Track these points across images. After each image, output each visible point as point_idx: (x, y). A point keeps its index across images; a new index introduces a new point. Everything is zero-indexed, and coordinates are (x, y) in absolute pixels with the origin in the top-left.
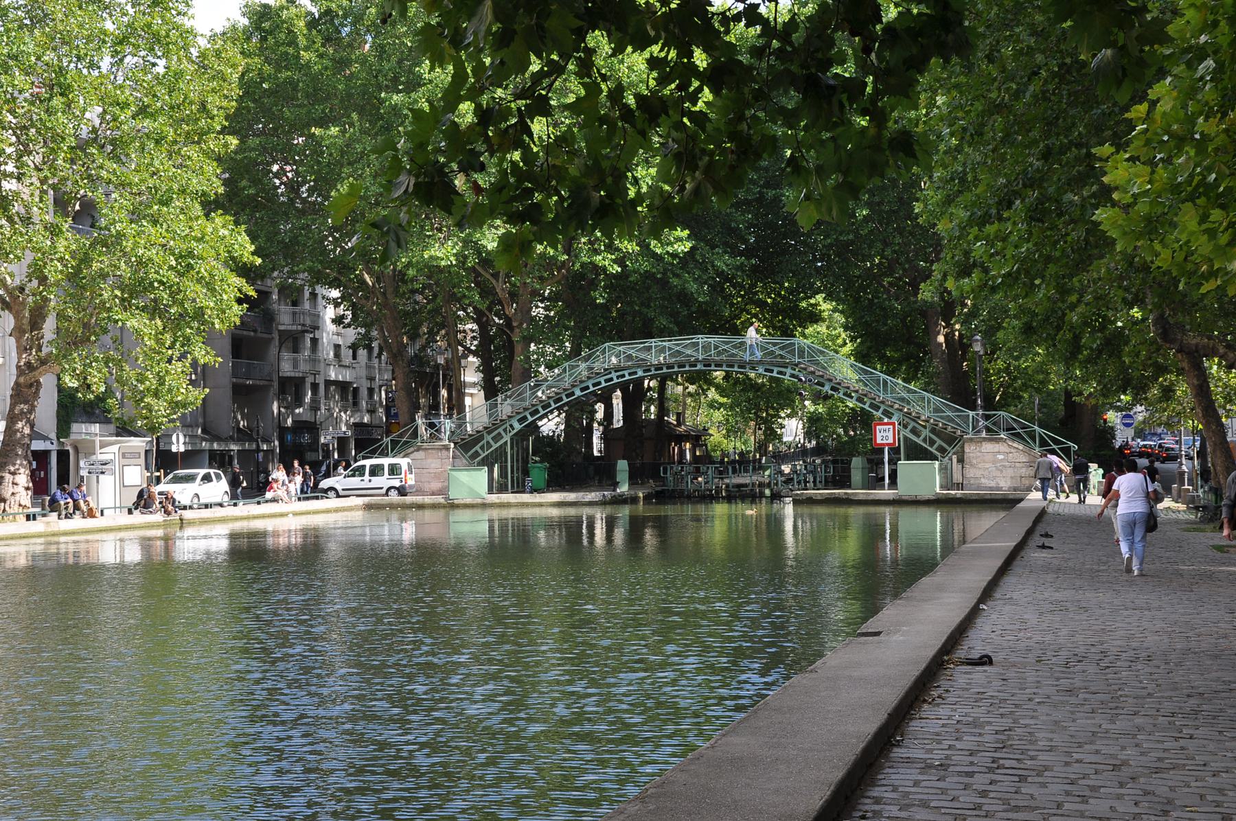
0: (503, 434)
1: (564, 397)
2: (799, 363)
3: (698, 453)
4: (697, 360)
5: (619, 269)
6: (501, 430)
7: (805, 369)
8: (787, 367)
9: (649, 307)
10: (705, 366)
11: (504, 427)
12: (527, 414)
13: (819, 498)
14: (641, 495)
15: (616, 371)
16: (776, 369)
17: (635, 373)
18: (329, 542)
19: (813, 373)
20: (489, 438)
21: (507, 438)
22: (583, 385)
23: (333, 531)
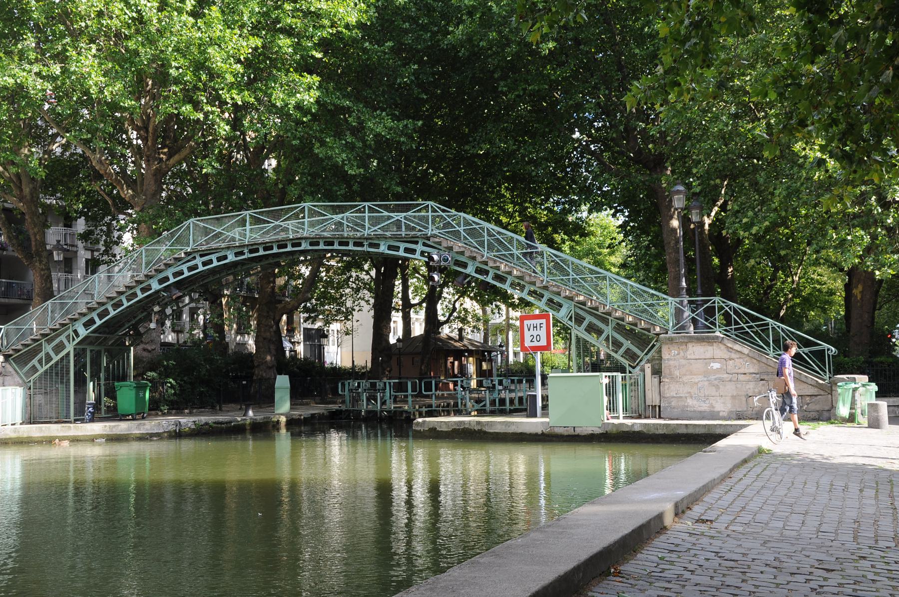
0: (38, 366)
1: (139, 293)
6: (63, 338)
7: (440, 243)
8: (416, 243)
10: (311, 244)
11: (66, 334)
12: (94, 315)
13: (445, 429)
15: (201, 256)
16: (403, 246)
17: (225, 257)
19: (450, 249)
20: (48, 348)
21: (70, 348)
22: (161, 276)
23: (27, 416)
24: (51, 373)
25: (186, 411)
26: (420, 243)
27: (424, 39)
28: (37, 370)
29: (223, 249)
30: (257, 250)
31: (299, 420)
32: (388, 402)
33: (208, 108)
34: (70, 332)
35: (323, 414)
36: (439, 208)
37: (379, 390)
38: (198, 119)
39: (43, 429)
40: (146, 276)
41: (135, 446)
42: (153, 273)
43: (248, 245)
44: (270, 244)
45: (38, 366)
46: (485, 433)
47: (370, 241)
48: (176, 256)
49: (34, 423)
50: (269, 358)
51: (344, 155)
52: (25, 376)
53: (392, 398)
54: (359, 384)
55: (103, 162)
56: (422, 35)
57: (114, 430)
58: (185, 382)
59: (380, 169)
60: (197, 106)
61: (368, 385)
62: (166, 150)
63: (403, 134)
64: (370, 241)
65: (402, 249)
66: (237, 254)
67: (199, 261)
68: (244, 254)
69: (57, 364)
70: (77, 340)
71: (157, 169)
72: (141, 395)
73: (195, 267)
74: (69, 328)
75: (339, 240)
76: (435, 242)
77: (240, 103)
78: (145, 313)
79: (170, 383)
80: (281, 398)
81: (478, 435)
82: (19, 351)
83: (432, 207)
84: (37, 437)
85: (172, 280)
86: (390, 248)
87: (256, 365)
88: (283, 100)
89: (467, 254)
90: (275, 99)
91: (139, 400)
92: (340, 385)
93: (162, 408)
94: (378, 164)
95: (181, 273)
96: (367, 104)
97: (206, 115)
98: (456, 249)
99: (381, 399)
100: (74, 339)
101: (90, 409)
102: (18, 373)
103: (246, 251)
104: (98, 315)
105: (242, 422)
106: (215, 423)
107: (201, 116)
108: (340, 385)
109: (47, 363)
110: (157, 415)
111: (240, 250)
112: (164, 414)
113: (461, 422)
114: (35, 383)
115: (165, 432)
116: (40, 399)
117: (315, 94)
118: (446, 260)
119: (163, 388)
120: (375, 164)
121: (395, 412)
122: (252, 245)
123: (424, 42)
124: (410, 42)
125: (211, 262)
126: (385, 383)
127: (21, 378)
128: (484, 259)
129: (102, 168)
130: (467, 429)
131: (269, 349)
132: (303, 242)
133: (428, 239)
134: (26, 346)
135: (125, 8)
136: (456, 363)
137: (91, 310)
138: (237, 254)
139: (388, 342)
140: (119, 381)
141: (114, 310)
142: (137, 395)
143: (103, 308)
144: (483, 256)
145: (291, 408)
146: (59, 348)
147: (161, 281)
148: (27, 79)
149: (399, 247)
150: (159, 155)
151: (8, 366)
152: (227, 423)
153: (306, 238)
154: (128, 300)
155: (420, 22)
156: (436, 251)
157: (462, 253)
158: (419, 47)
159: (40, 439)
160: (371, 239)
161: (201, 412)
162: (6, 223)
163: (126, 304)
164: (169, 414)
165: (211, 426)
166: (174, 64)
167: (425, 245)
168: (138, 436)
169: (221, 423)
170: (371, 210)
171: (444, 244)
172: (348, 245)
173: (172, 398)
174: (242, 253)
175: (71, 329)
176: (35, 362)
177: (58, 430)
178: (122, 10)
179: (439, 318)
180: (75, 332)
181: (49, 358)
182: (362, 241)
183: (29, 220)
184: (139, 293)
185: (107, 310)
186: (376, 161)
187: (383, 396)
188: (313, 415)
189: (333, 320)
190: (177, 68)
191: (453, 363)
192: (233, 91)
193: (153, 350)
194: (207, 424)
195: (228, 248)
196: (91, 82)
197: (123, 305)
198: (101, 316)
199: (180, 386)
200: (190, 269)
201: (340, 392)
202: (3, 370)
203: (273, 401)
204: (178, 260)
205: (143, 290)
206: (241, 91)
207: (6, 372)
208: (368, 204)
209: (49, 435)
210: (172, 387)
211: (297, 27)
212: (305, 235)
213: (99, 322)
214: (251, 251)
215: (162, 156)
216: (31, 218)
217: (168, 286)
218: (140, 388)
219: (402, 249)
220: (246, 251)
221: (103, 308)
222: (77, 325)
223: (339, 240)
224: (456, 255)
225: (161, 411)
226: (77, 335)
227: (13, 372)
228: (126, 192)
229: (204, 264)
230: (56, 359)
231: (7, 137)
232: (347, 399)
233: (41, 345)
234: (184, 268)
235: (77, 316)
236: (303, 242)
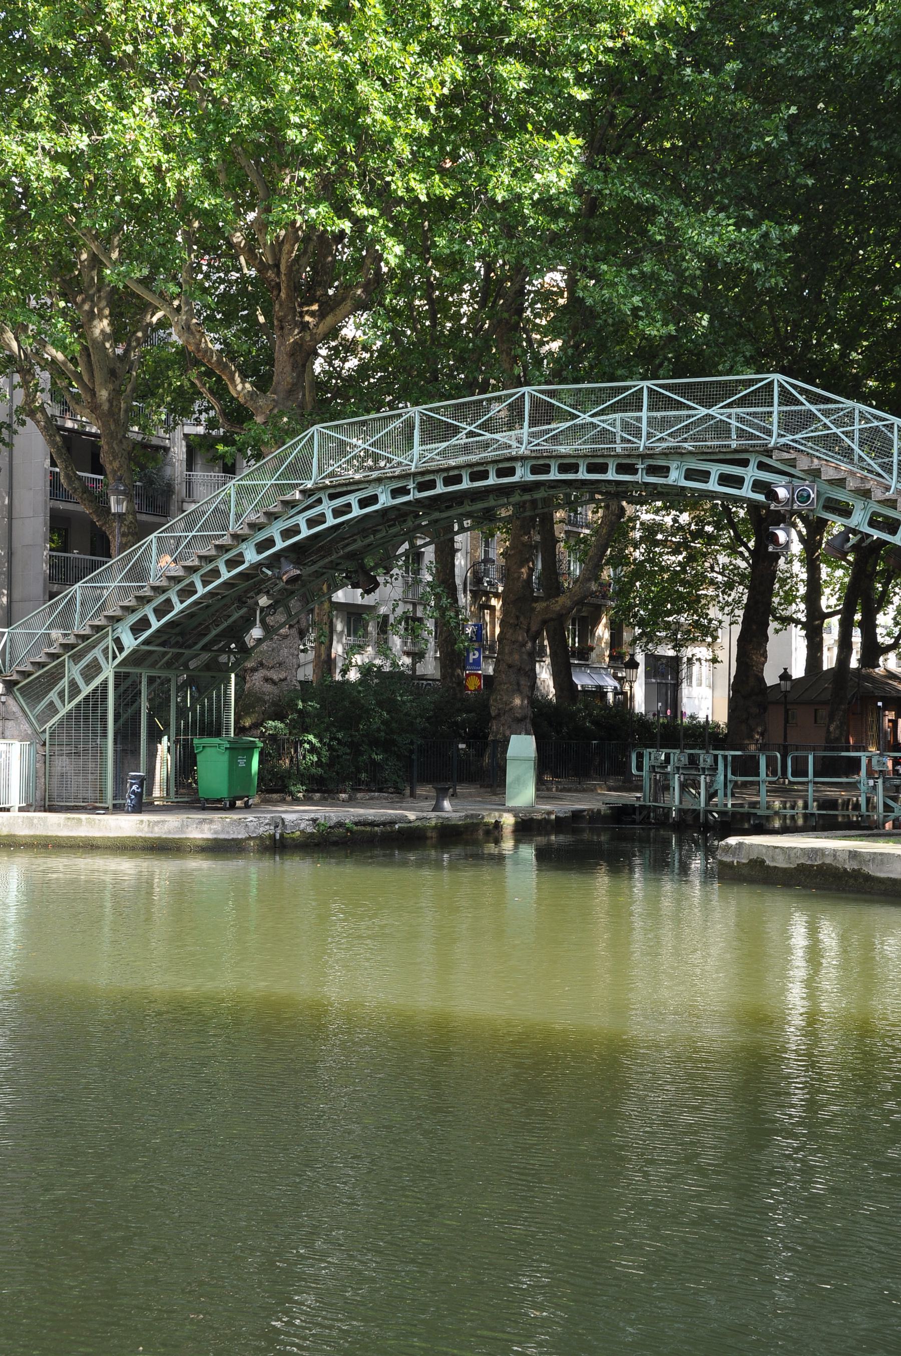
0: (58, 703)
1: (223, 569)
6: (97, 652)
7: (792, 463)
8: (744, 463)
10: (535, 470)
11: (102, 645)
12: (148, 611)
13: (781, 863)
15: (332, 497)
16: (716, 470)
17: (374, 499)
18: (483, 818)
19: (815, 473)
20: (74, 671)
21: (108, 673)
22: (262, 536)
23: (38, 794)
24: (77, 718)
25: (343, 796)
26: (753, 464)
27: (812, 55)
28: (56, 711)
30: (431, 485)
31: (547, 821)
32: (721, 793)
33: (363, 211)
34: (109, 642)
35: (599, 811)
36: (802, 391)
37: (704, 769)
38: (342, 232)
39: (35, 821)
40: (235, 536)
41: (198, 864)
42: (246, 531)
43: (415, 475)
44: (456, 472)
45: (58, 703)
46: (868, 878)
48: (287, 497)
49: (51, 809)
50: (517, 701)
51: (636, 300)
52: (38, 721)
53: (730, 786)
54: (668, 756)
55: (192, 327)
56: (808, 46)
57: (156, 829)
58: (340, 742)
59: (715, 333)
60: (342, 208)
61: (685, 760)
62: (315, 307)
63: (759, 255)
65: (714, 478)
66: (395, 493)
67: (327, 507)
68: (407, 492)
69: (87, 698)
70: (120, 658)
71: (295, 342)
72: (242, 763)
73: (320, 519)
74: (107, 634)
77: (423, 198)
78: (244, 610)
79: (309, 742)
80: (518, 779)
81: (852, 881)
82: (28, 674)
83: (781, 385)
84: (25, 837)
85: (280, 545)
86: (690, 475)
87: (493, 714)
88: (509, 189)
89: (852, 484)
90: (494, 188)
91: (237, 774)
92: (634, 757)
93: (292, 788)
94: (711, 321)
95: (295, 530)
96: (686, 197)
97: (359, 223)
98: (829, 473)
99: (708, 786)
100: (114, 657)
101: (134, 787)
102: (27, 716)
104: (156, 611)
105: (418, 823)
106: (356, 824)
107: (346, 225)
108: (634, 757)
109: (72, 698)
110: (283, 801)
111: (400, 484)
112: (296, 801)
113: (815, 851)
114: (52, 735)
115: (250, 838)
116: (62, 764)
117: (570, 170)
118: (804, 498)
119: (296, 751)
120: (705, 323)
121: (734, 814)
122: (422, 474)
123: (811, 62)
124: (781, 61)
126: (716, 757)
127: (31, 724)
128: (889, 495)
129: (192, 341)
131: (518, 684)
132: (518, 465)
133: (768, 453)
134: (40, 665)
135: (208, 14)
137: (143, 600)
138: (395, 493)
139: (762, 680)
140: (202, 734)
141: (182, 602)
142: (232, 763)
143: (162, 598)
144: (888, 489)
145: (537, 797)
146: (92, 670)
147: (261, 547)
148: (23, 160)
149: (708, 473)
150: (302, 316)
151: (11, 702)
152: (384, 824)
153: (523, 458)
154: (205, 583)
155: (807, 18)
156: (784, 480)
157: (840, 483)
158: (801, 73)
159: (29, 840)
160: (651, 456)
161: (372, 798)
162: (64, 451)
163: (201, 591)
164: (308, 800)
165: (348, 830)
166: (294, 119)
167: (762, 466)
168: (200, 843)
169: (372, 824)
171: (803, 463)
173: (313, 770)
174: (404, 491)
175: (110, 638)
176: (53, 695)
177: (59, 825)
178: (202, 18)
179: (880, 639)
180: (118, 641)
181: (74, 689)
183: (106, 447)
184: (223, 569)
185: (168, 601)
186: (706, 317)
187: (712, 782)
188: (577, 815)
189: (687, 640)
190: (299, 127)
192: (412, 175)
193: (281, 680)
194: (340, 824)
196: (139, 162)
197: (196, 592)
198: (160, 612)
199: (331, 748)
200: (311, 523)
201: (634, 771)
202: (3, 709)
203: (502, 783)
204: (289, 504)
205: (231, 564)
206: (428, 176)
207: (7, 712)
209: (44, 833)
210: (313, 750)
211: (539, 37)
212: (523, 450)
213: (155, 624)
214: (422, 487)
215: (307, 318)
216: (108, 443)
217: (274, 554)
218: (240, 750)
219: (714, 478)
221: (162, 598)
222: (119, 630)
225: (291, 794)
226: (121, 649)
227: (19, 714)
228: (239, 387)
229: (337, 513)
230: (86, 690)
231: (12, 279)
232: (646, 784)
233: (62, 664)
234: (301, 520)
235: (119, 613)
236: (518, 465)
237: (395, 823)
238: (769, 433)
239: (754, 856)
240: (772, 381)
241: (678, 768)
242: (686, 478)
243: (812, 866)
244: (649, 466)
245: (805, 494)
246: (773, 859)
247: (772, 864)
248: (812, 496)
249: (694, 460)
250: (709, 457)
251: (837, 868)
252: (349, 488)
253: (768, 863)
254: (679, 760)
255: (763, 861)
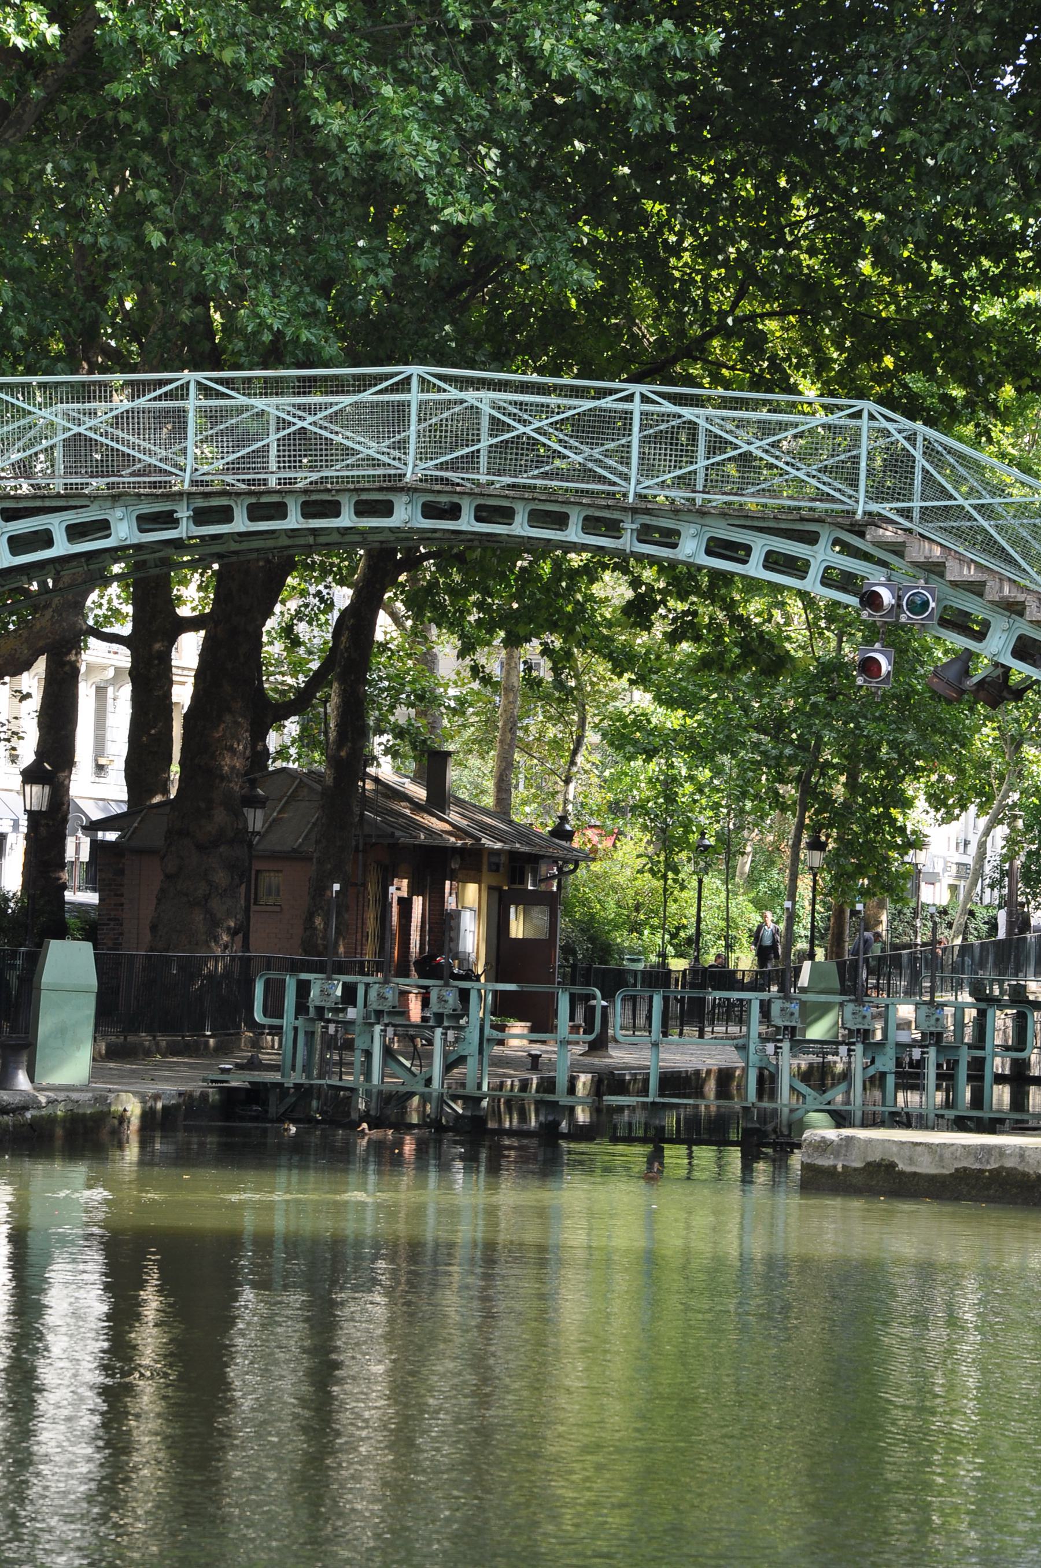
2: (875, 520)
3: (517, 929)
4: (394, 485)
5: (52, 32)
7: (897, 549)
8: (811, 539)
9: (213, 234)
10: (430, 511)
13: (926, 1166)
14: (133, 1107)
16: (760, 545)
19: (934, 569)
26: (824, 541)
29: (93, 498)
35: (204, 1096)
47: (647, 520)
64: (647, 520)
65: (757, 557)
66: (146, 522)
75: (303, 498)
76: (880, 544)
80: (62, 1032)
86: (717, 548)
89: (992, 592)
98: (956, 572)
103: (183, 513)
113: (988, 1150)
125: (45, 539)
130: (1012, 1172)
136: (418, 903)
149: (748, 549)
153: (410, 490)
157: (976, 589)
160: (647, 512)
170: (206, 391)
172: (456, 517)
182: (616, 515)
191: (405, 905)
195: (116, 498)
201: (258, 1016)
208: (200, 376)
220: (183, 513)
223: (303, 498)
224: (949, 590)
237: (26, 1108)
238: (627, 479)
239: (875, 1157)
240: (409, 377)
241: (379, 1014)
242: (709, 552)
243: (981, 1171)
244: (643, 525)
245: (918, 600)
246: (911, 1161)
247: (909, 1169)
248: (932, 605)
249: (723, 523)
250: (749, 523)
251: (1025, 1174)
252: (47, 503)
253: (901, 1166)
254: (381, 997)
255: (893, 1165)
